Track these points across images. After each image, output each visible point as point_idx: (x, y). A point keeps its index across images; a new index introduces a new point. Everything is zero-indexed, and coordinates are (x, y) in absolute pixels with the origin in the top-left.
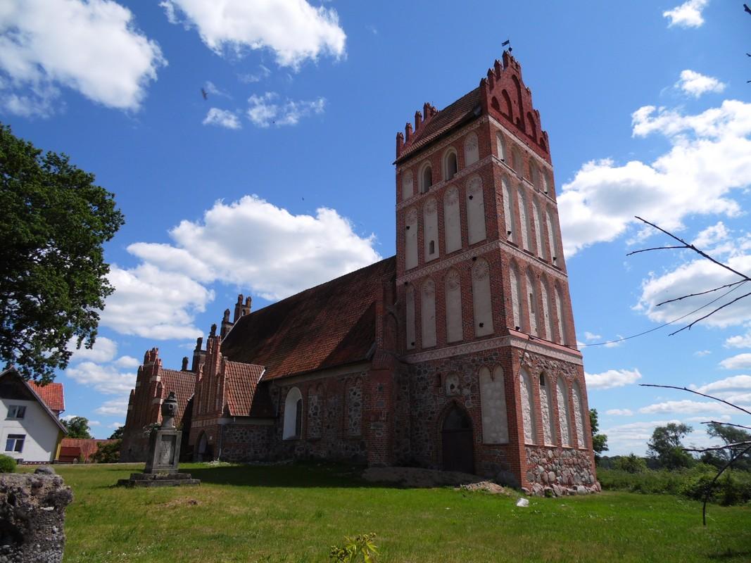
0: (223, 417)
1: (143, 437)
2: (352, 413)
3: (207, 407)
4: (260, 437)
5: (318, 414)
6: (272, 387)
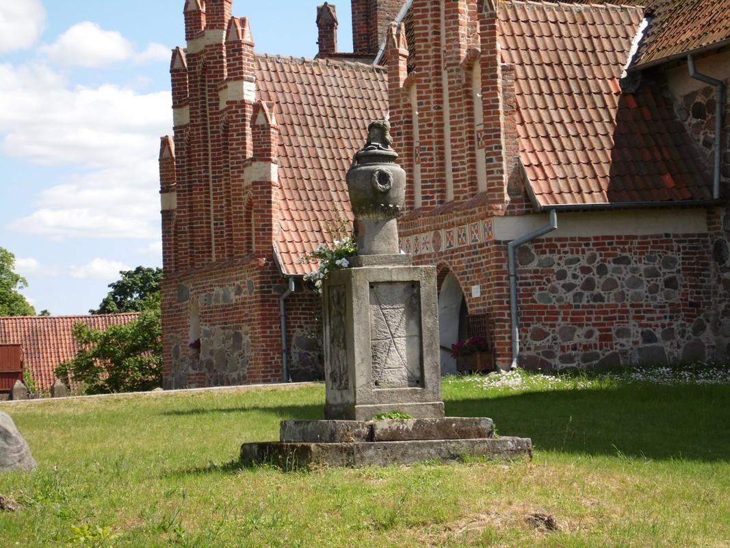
0: (510, 212)
1: (233, 297)
3: (442, 182)
4: (660, 282)
6: (686, 87)
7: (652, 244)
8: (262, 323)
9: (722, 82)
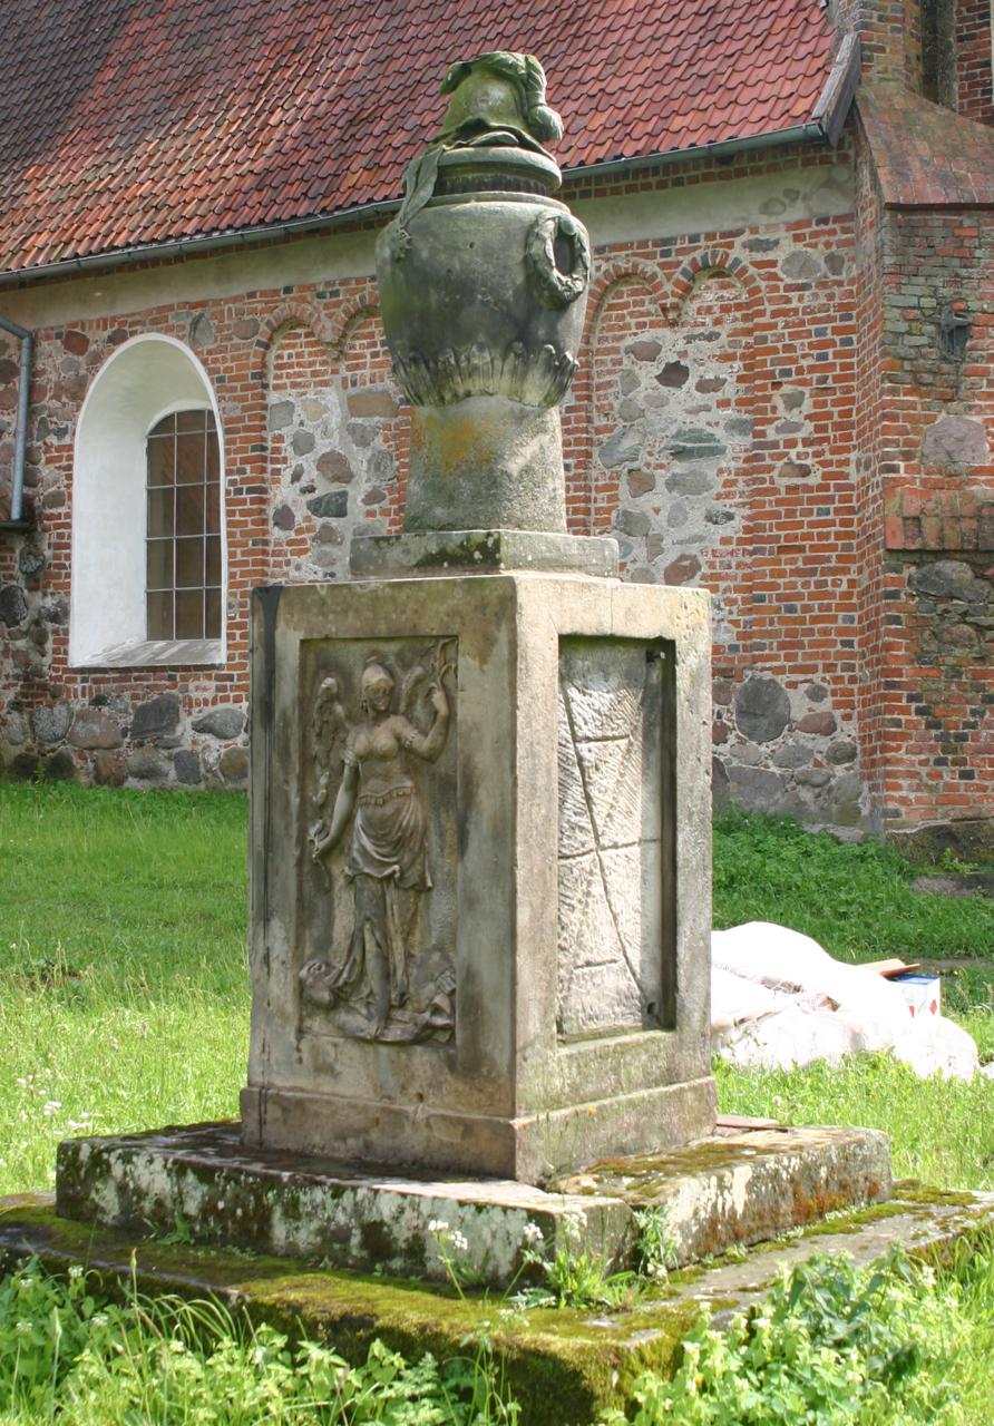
2: (658, 500)
5: (356, 504)
7: (836, 418)
8: (752, 505)
9: (30, 334)
